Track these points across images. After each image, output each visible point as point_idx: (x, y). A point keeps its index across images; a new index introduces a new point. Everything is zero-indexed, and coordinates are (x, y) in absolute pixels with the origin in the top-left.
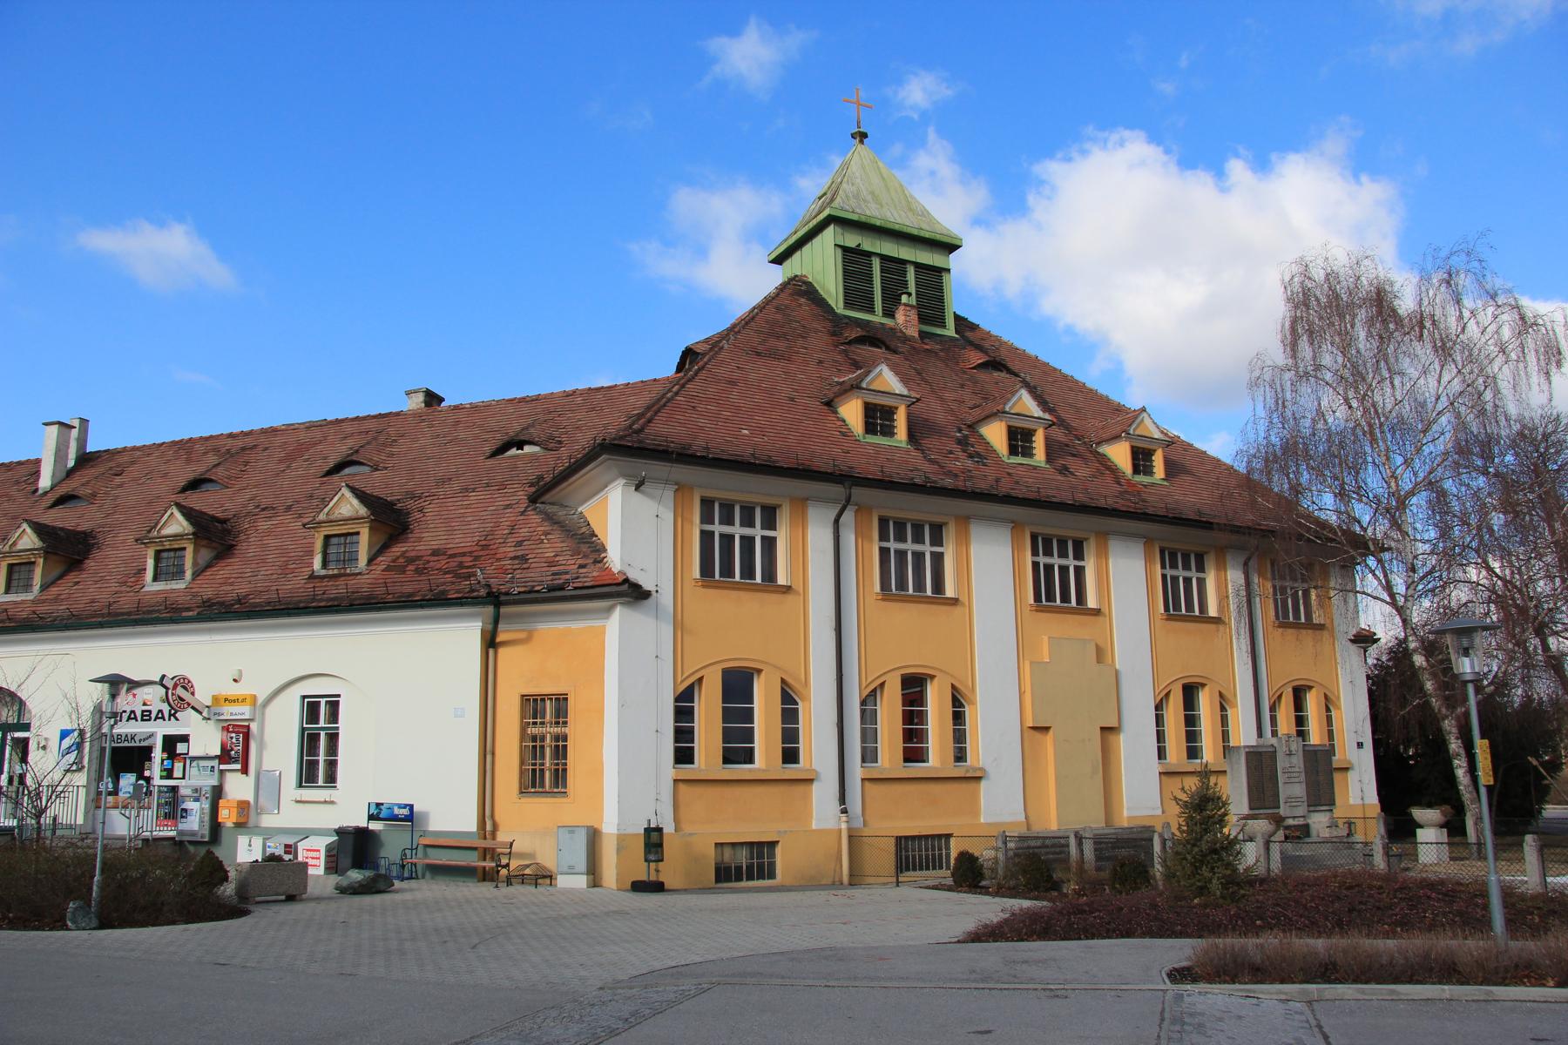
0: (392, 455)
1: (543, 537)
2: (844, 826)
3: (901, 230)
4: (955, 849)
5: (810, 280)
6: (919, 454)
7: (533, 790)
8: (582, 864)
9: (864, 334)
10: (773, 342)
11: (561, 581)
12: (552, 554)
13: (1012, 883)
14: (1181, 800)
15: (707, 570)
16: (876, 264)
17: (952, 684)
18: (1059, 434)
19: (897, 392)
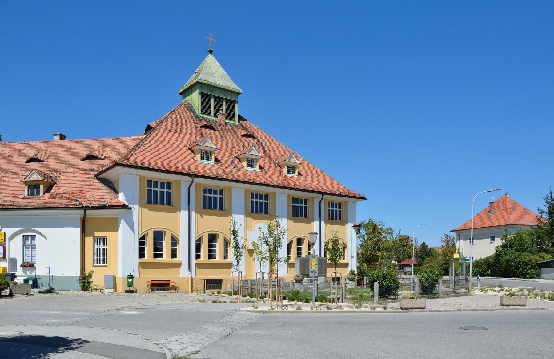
0: (49, 157)
11: (105, 204)
12: (102, 195)
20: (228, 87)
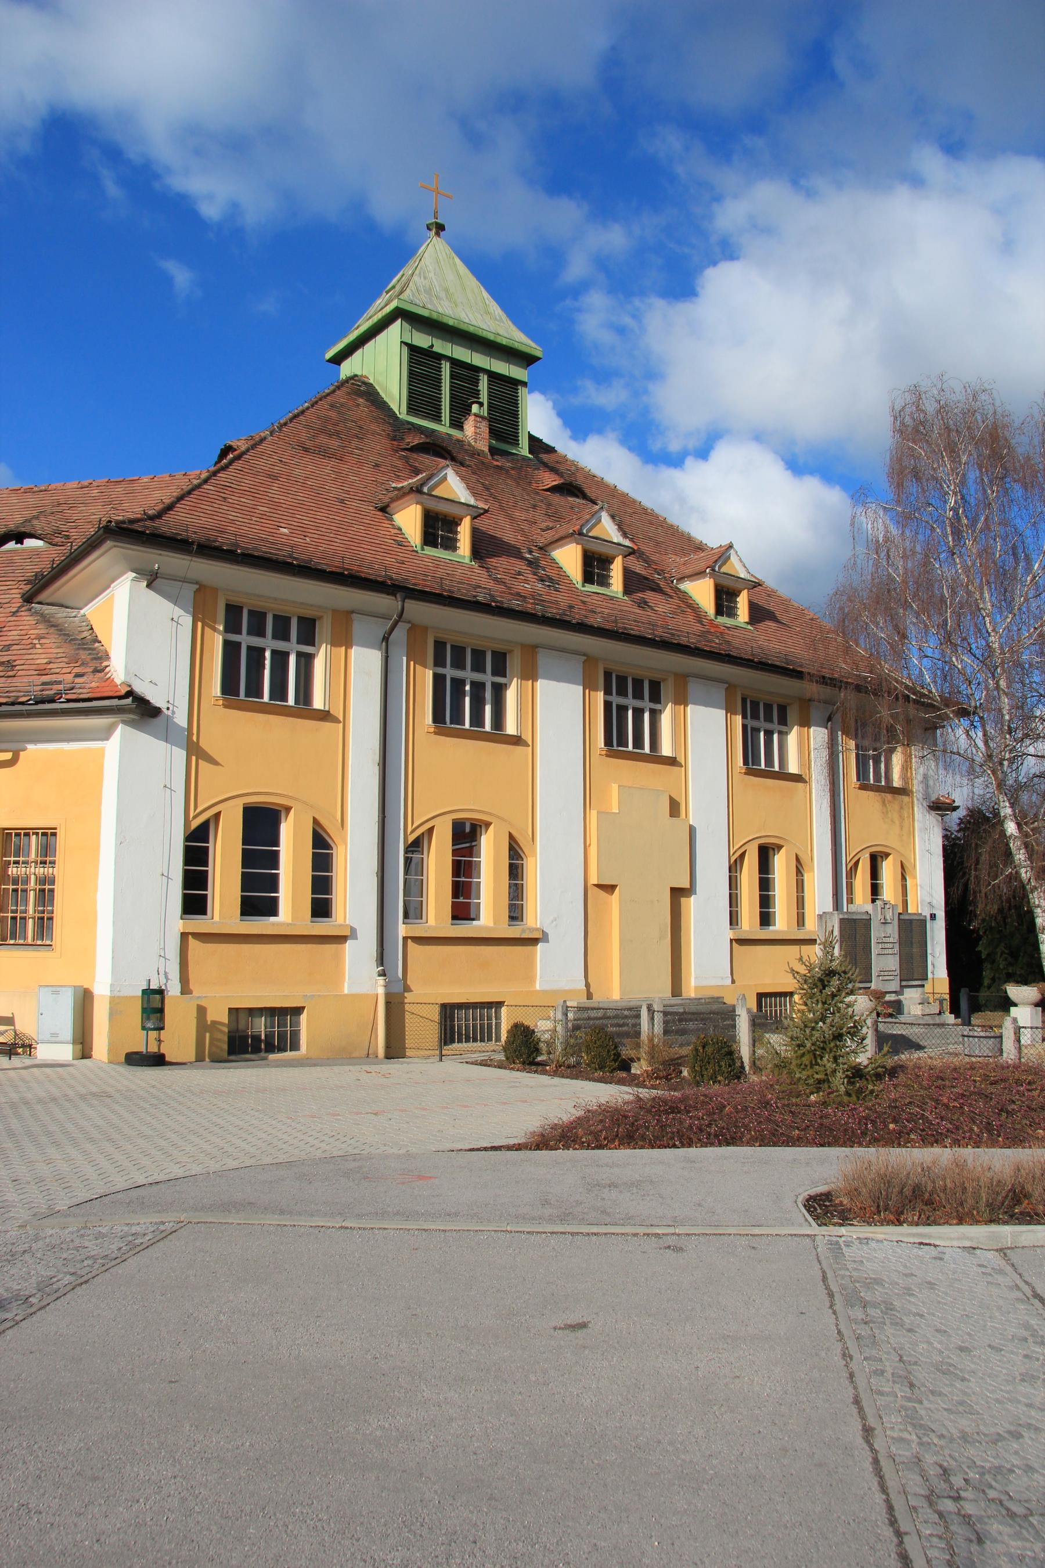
1: (36, 641)
2: (381, 991)
3: (477, 333)
4: (506, 1021)
5: (371, 381)
6: (484, 572)
7: (12, 942)
8: (67, 1030)
9: (428, 441)
10: (323, 439)
11: (52, 692)
12: (45, 661)
13: (572, 1060)
14: (798, 973)
15: (229, 687)
16: (446, 368)
18: (638, 567)
19: (463, 501)
20: (498, 334)
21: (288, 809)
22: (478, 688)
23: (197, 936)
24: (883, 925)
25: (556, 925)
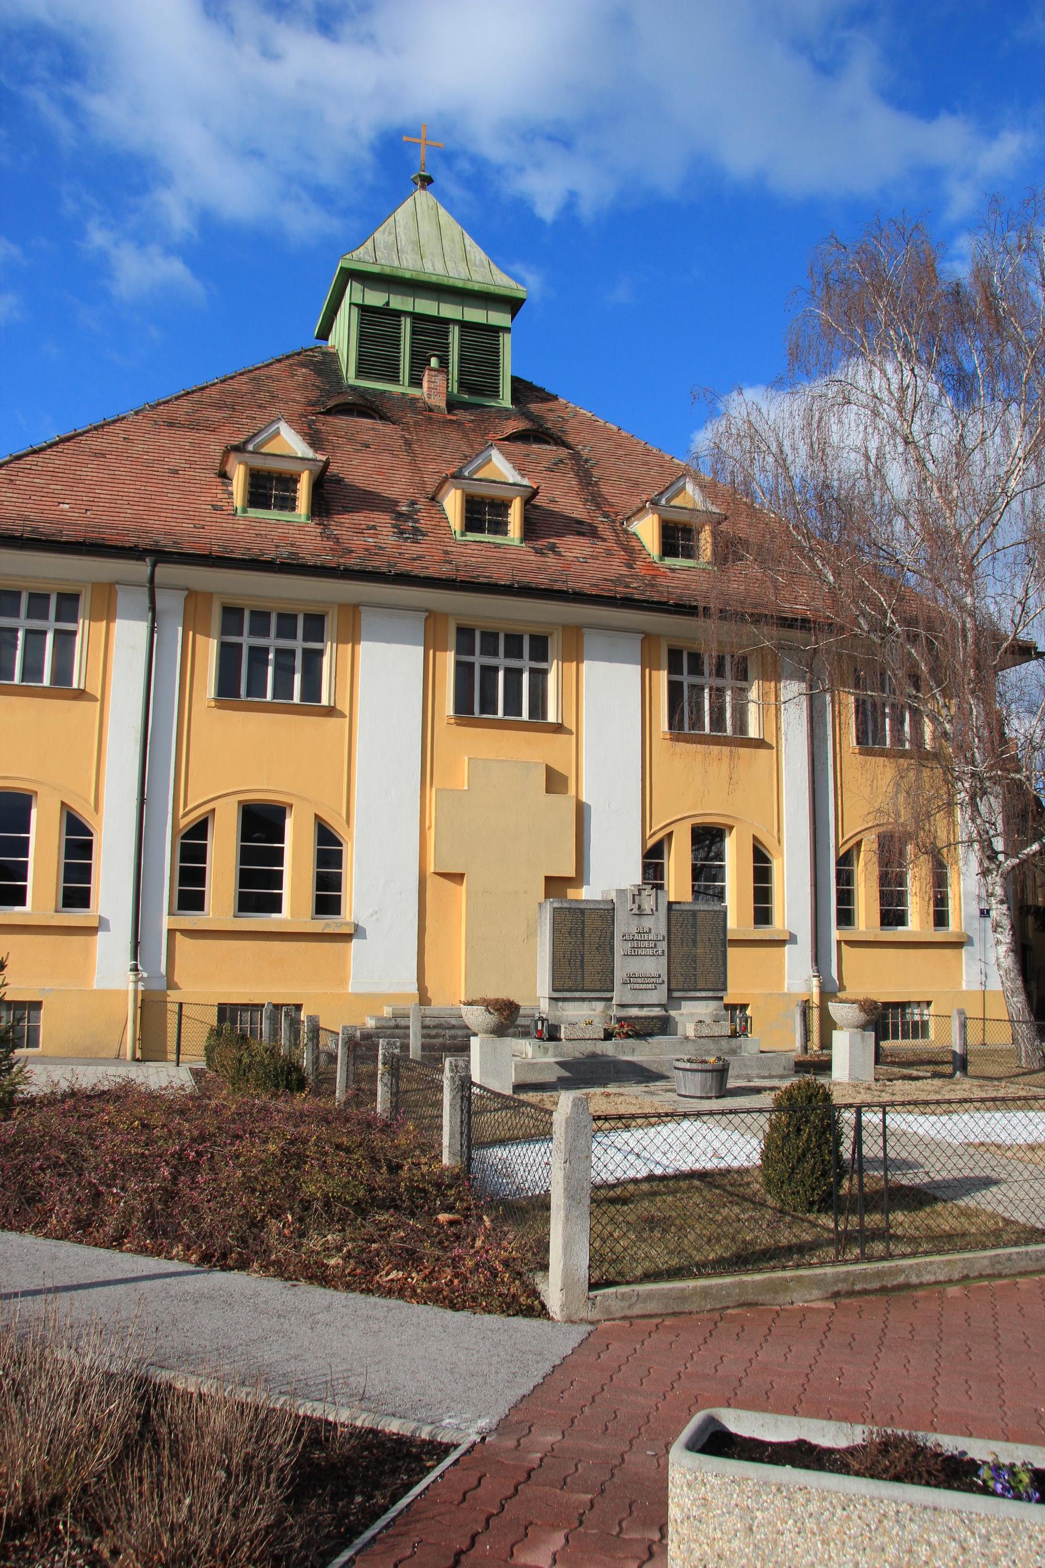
3: (441, 282)
15: (463, 706)
16: (406, 325)
17: (754, 836)
21: (731, 828)
22: (285, 656)
23: (848, 943)
24: (637, 918)
25: (377, 920)
